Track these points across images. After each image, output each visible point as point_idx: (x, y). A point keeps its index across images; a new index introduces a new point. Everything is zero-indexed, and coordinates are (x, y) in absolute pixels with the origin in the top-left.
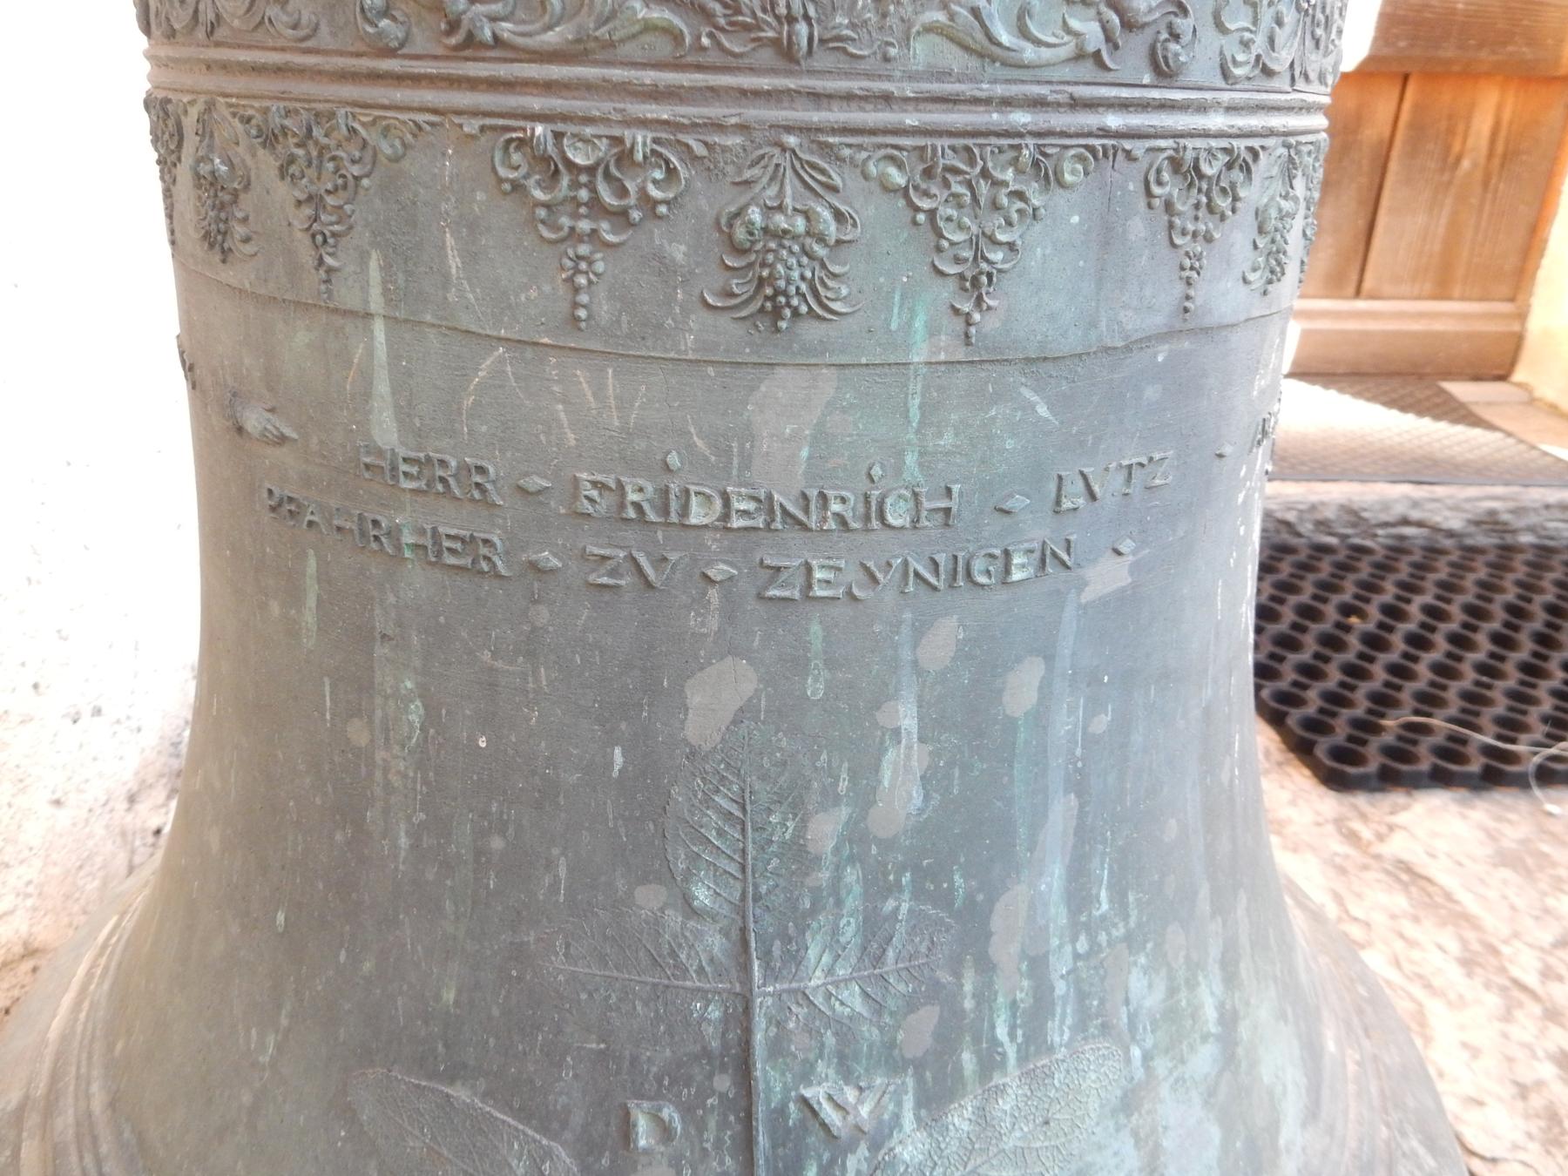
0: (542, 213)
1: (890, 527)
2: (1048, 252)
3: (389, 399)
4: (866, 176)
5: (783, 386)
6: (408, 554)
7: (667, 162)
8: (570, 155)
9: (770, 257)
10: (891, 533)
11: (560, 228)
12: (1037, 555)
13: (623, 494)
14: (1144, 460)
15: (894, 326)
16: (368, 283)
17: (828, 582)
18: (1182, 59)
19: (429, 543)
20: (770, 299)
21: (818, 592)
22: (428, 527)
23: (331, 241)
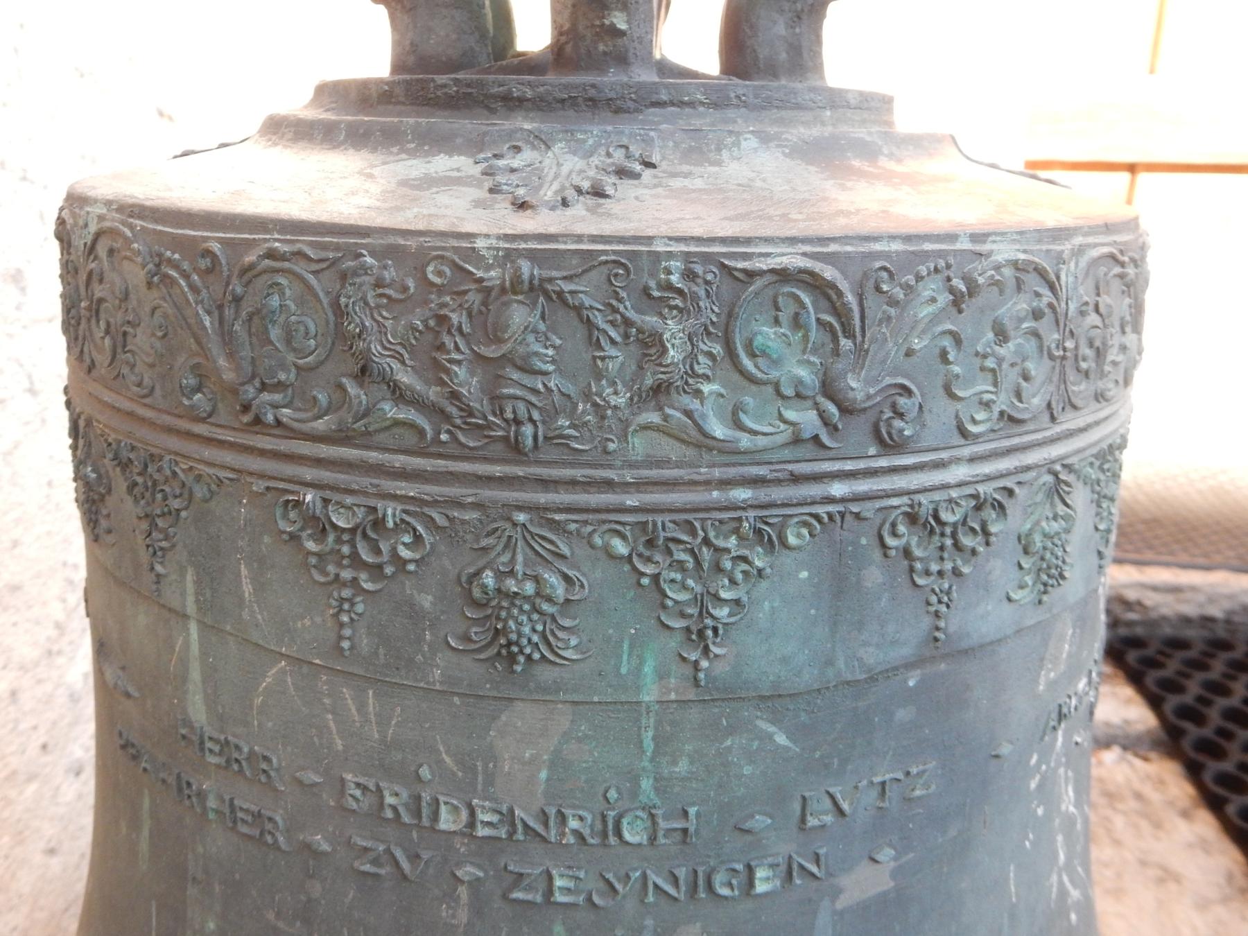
0: (313, 560)
1: (627, 843)
2: (776, 604)
3: (200, 685)
4: (592, 547)
5: (522, 716)
6: (211, 816)
7: (415, 530)
8: (334, 520)
9: (503, 614)
10: (629, 849)
11: (327, 574)
12: (783, 868)
13: (382, 797)
14: (900, 775)
15: (624, 670)
16: (185, 591)
17: (569, 890)
18: (906, 433)
19: (227, 811)
20: (505, 653)
21: (559, 898)
22: (227, 798)
23: (159, 553)
